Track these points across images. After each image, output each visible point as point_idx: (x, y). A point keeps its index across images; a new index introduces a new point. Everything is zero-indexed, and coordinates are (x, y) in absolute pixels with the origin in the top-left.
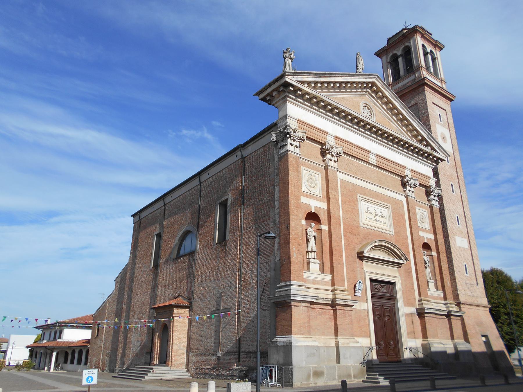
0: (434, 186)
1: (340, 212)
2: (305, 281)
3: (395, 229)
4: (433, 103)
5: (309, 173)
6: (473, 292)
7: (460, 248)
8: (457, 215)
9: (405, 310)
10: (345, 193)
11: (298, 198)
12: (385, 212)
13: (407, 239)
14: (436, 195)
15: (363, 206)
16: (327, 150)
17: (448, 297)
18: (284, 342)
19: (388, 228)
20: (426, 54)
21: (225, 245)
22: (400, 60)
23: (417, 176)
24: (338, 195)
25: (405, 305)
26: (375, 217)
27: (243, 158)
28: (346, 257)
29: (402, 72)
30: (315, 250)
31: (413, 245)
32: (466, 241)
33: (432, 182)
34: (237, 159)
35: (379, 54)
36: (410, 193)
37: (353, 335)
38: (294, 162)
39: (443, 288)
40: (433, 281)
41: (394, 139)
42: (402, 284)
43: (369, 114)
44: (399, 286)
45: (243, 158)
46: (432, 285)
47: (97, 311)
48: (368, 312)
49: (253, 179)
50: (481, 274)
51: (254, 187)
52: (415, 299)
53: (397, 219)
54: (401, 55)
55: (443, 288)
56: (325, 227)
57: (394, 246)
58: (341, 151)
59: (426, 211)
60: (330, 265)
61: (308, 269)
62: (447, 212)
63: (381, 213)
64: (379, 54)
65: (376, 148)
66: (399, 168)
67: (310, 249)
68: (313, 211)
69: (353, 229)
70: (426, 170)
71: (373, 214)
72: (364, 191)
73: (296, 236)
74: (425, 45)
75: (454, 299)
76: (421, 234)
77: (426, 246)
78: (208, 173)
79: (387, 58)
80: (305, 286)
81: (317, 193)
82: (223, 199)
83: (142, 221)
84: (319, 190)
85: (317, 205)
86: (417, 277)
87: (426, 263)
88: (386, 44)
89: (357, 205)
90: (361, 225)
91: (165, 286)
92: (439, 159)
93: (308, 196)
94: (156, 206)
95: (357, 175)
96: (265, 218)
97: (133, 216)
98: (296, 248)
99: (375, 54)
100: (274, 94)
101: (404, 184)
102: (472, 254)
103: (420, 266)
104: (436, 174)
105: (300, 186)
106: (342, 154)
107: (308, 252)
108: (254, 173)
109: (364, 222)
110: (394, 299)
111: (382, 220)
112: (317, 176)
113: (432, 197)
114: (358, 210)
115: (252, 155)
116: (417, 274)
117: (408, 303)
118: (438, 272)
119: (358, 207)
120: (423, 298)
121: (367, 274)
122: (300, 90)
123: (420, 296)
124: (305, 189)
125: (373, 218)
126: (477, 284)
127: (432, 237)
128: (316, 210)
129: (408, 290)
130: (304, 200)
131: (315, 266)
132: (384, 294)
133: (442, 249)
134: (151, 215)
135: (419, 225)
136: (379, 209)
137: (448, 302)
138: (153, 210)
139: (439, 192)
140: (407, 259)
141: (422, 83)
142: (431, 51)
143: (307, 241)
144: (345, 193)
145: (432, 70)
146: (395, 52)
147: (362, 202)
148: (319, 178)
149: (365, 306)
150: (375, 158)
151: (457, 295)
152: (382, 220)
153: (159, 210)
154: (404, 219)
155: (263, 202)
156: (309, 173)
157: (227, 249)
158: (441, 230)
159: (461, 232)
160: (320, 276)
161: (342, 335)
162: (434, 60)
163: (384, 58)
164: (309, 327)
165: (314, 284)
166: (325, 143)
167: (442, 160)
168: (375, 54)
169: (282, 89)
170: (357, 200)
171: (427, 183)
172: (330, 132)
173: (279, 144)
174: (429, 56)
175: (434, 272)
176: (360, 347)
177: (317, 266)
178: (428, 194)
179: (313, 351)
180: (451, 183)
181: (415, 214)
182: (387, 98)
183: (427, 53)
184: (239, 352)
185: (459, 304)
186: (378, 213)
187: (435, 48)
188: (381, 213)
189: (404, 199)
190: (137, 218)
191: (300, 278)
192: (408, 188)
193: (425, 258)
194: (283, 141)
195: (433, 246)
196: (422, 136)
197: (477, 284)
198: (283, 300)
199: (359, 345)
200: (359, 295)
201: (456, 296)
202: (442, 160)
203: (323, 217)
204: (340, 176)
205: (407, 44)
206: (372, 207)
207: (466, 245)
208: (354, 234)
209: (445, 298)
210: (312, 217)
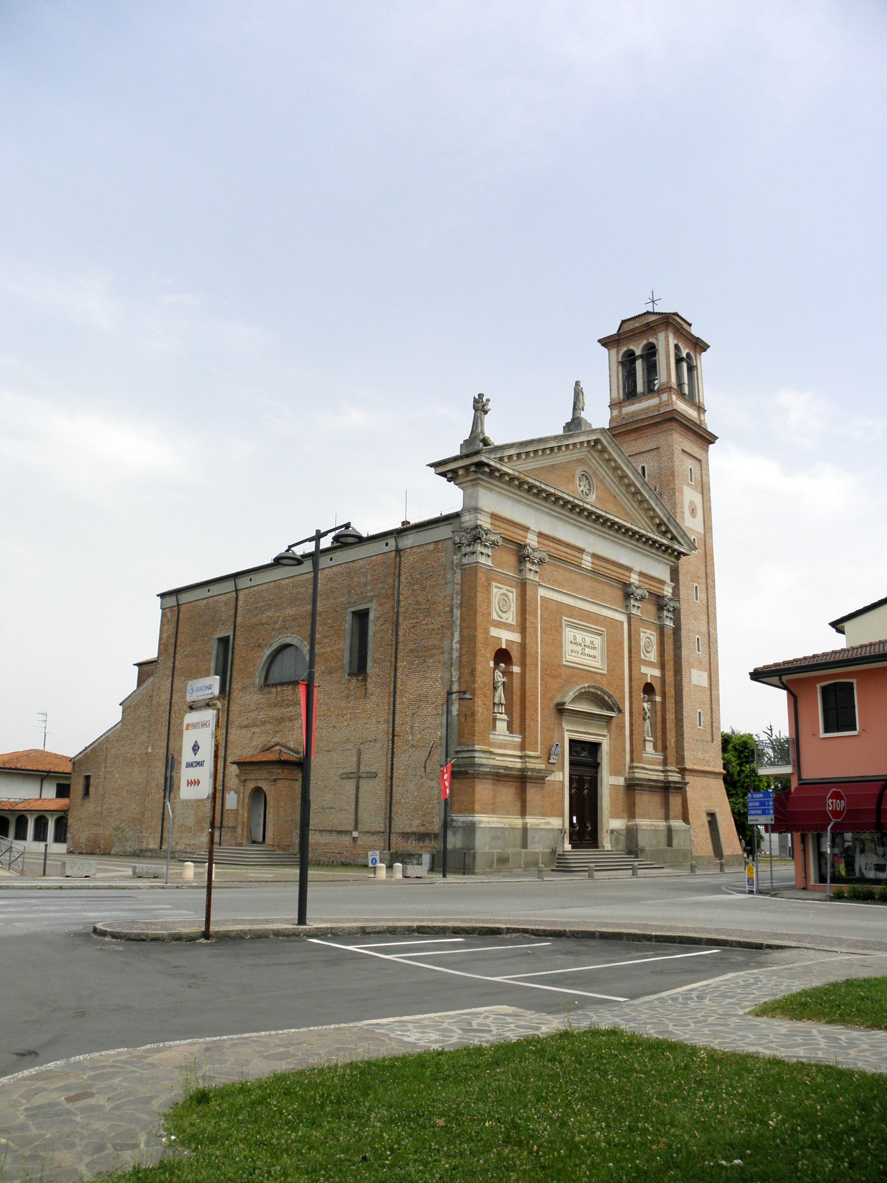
0: (670, 595)
1: (538, 648)
2: (490, 744)
3: (608, 665)
4: (683, 451)
5: (502, 591)
6: (705, 756)
7: (696, 686)
8: (698, 636)
9: (610, 781)
10: (546, 616)
11: (487, 631)
12: (597, 641)
13: (623, 679)
14: (671, 609)
15: (569, 634)
16: (528, 556)
17: (669, 761)
18: (462, 822)
19: (598, 665)
20: (679, 360)
21: (365, 680)
22: (639, 364)
23: (647, 581)
24: (537, 622)
25: (611, 774)
26: (582, 651)
27: (398, 551)
28: (542, 710)
29: (640, 388)
30: (503, 701)
31: (631, 687)
32: (705, 675)
33: (668, 591)
34: (387, 549)
35: (606, 342)
36: (634, 611)
37: (544, 815)
38: (483, 579)
39: (664, 749)
40: (651, 739)
41: (608, 461)
42: (610, 744)
43: (587, 487)
44: (605, 748)
45: (398, 551)
46: (649, 747)
47: (81, 753)
48: (563, 785)
49: (415, 587)
50: (720, 739)
51: (417, 601)
52: (625, 765)
53: (612, 649)
54: (641, 356)
55: (664, 749)
56: (516, 669)
57: (605, 693)
58: (544, 555)
59: (654, 633)
60: (520, 724)
61: (494, 727)
62: (683, 632)
63: (592, 642)
64: (606, 342)
65: (593, 544)
66: (622, 571)
67: (496, 701)
68: (504, 647)
69: (556, 671)
70: (661, 571)
71: (580, 645)
72: (571, 611)
73: (482, 685)
74: (680, 345)
75: (677, 763)
76: (644, 669)
77: (648, 689)
78: (330, 556)
79: (618, 353)
80: (491, 753)
81: (510, 621)
82: (361, 607)
83: (183, 608)
84: (511, 617)
85: (507, 637)
86: (631, 735)
87: (646, 714)
88: (615, 332)
89: (561, 634)
90: (565, 663)
91: (242, 727)
92: (680, 553)
93: (500, 625)
94: (216, 589)
95: (564, 587)
96: (435, 651)
97: (162, 596)
98: (482, 701)
99: (599, 341)
100: (461, 472)
101: (627, 596)
102: (711, 695)
103: (638, 718)
104: (675, 574)
105: (490, 614)
106: (547, 559)
107: (494, 704)
108: (418, 579)
109: (569, 658)
110: (596, 766)
111: (592, 652)
112: (511, 594)
113: (665, 613)
114: (561, 642)
115: (414, 550)
116: (631, 730)
117: (615, 772)
118: (659, 725)
119: (561, 637)
120: (635, 764)
121: (566, 733)
122: (498, 470)
123: (632, 760)
124: (495, 616)
125: (580, 652)
126: (713, 740)
127: (657, 673)
128: (507, 645)
129: (617, 751)
130: (494, 632)
131: (502, 726)
132: (585, 756)
133: (670, 691)
134: (204, 602)
135: (643, 657)
136: (589, 638)
137: (669, 768)
138: (209, 594)
139: (676, 605)
140: (620, 711)
141: (669, 417)
142: (688, 355)
143: (495, 689)
144: (546, 616)
145: (686, 390)
146: (632, 347)
147: (568, 629)
148: (513, 595)
149: (562, 777)
150: (590, 559)
151: (683, 758)
152: (592, 652)
153: (224, 598)
154: (623, 650)
155: (432, 626)
156: (502, 591)
157: (368, 686)
158: (672, 663)
159: (701, 662)
160: (508, 738)
161: (530, 815)
162: (691, 369)
163: (614, 351)
164: (494, 804)
165: (500, 748)
166: (525, 546)
167: (685, 554)
168: (599, 341)
169: (473, 469)
170: (561, 626)
171: (660, 591)
172: (533, 527)
173: (463, 548)
174: (685, 365)
175: (653, 726)
176: (552, 829)
177: (505, 724)
178: (661, 608)
179: (497, 833)
180: (696, 584)
181: (638, 641)
182: (615, 461)
183: (682, 359)
184: (390, 833)
185: (683, 771)
186: (588, 643)
187: (695, 348)
188: (592, 642)
189: (623, 618)
190: (172, 601)
191: (486, 741)
192: (633, 602)
193: (645, 705)
194: (469, 545)
195: (658, 689)
196: (661, 519)
197: (713, 740)
198: (463, 769)
199: (550, 827)
200: (555, 761)
201: (680, 759)
202: (685, 554)
203: (515, 654)
204: (542, 592)
205: (652, 340)
206: (580, 636)
207: (705, 683)
208: (554, 677)
209: (665, 762)
210: (502, 656)
